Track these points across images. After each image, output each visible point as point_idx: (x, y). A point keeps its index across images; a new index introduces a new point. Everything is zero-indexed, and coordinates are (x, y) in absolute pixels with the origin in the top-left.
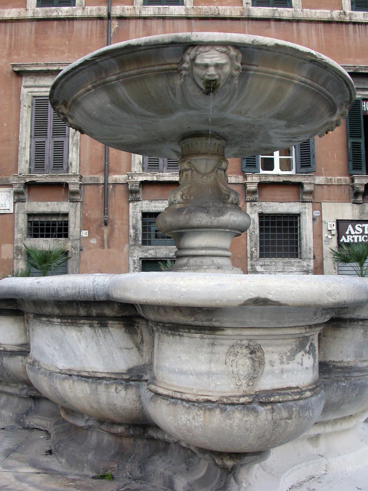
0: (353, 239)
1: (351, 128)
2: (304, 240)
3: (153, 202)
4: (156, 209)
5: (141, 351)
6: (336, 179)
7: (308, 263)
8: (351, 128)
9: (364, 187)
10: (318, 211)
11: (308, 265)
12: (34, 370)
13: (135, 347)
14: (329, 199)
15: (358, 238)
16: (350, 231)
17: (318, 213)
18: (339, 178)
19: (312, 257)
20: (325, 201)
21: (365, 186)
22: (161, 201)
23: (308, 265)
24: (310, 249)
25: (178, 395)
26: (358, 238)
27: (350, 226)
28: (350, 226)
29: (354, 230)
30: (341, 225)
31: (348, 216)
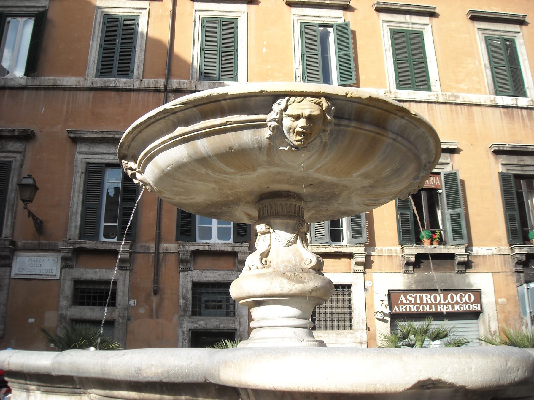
0: (406, 309)
3: (205, 271)
4: (207, 279)
9: (414, 257)
10: (370, 282)
15: (410, 308)
16: (402, 301)
17: (370, 284)
18: (389, 248)
22: (212, 271)
26: (410, 308)
27: (402, 296)
28: (402, 296)
29: (406, 299)
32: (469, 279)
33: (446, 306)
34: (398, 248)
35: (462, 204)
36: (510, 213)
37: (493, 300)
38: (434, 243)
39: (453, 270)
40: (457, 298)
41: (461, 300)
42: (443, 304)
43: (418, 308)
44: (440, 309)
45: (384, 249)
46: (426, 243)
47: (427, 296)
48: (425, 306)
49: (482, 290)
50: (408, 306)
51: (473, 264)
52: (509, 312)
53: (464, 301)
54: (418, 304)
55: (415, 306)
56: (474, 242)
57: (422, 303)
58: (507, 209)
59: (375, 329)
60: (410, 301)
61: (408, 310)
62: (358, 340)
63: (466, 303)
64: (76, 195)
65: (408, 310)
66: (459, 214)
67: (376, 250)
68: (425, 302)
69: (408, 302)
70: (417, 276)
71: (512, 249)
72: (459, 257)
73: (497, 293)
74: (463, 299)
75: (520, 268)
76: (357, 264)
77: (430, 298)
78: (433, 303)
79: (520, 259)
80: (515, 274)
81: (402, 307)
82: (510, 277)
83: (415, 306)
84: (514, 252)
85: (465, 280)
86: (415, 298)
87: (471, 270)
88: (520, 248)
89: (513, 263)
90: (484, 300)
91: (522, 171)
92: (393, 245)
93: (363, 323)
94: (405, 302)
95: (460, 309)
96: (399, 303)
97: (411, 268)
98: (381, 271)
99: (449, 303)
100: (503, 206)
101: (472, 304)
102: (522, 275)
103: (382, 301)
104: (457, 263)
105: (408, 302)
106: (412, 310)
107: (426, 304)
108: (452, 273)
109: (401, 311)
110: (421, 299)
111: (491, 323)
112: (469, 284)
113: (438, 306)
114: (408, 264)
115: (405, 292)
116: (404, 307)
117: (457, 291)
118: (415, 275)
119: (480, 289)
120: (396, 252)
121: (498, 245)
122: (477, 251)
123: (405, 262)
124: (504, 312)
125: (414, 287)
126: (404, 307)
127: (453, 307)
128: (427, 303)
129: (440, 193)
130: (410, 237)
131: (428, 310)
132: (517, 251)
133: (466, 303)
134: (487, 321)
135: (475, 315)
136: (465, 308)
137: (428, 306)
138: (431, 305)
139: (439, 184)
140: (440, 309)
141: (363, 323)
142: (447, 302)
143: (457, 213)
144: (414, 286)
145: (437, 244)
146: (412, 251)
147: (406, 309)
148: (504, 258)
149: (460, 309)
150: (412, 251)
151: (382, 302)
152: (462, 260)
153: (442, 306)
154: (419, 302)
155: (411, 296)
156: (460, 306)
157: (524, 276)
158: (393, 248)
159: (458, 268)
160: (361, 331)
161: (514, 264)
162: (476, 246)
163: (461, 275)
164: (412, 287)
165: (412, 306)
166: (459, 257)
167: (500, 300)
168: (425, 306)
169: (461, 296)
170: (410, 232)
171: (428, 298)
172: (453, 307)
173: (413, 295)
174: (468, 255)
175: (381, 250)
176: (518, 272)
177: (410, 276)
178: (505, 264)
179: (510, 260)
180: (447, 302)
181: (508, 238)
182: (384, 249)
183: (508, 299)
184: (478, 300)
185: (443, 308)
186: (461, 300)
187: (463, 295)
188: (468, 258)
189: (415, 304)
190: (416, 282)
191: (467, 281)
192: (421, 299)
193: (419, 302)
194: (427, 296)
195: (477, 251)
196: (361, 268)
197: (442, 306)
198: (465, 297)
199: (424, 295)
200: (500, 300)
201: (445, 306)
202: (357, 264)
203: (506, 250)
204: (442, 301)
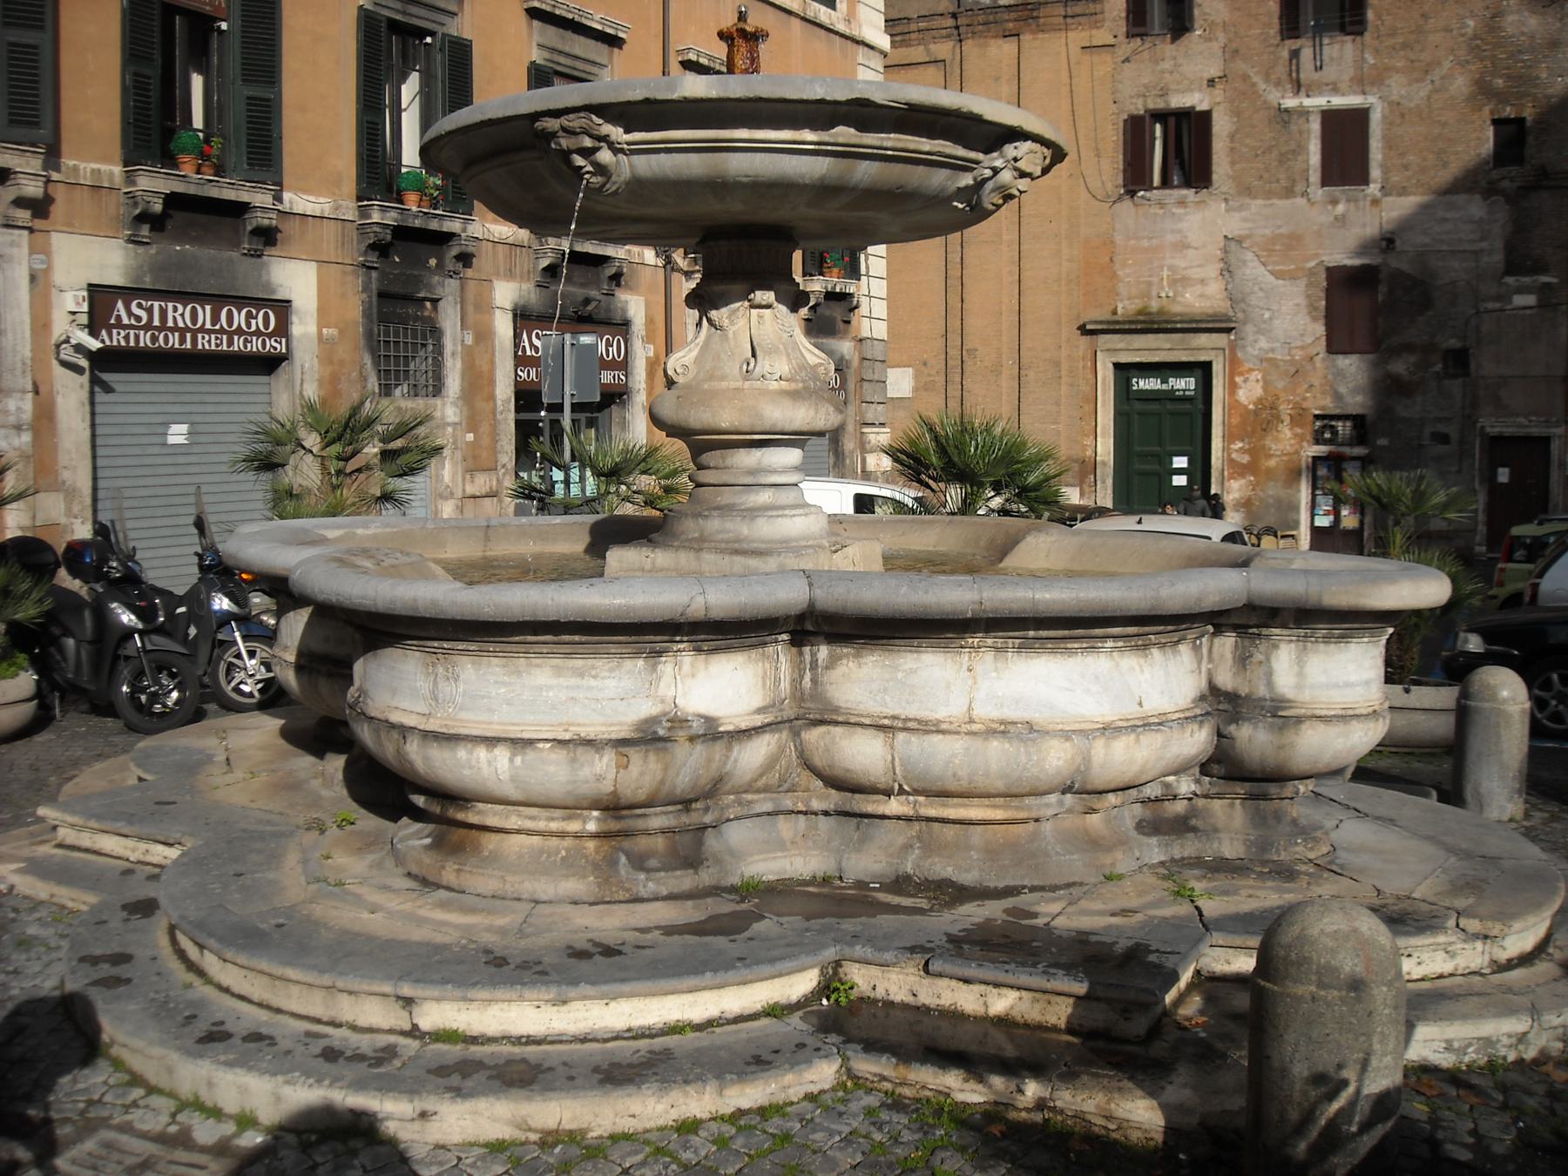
0: (127, 338)
1: (33, 109)
2: (10, 335)
5: (562, 94)
6: (88, 170)
7: (21, 404)
8: (33, 109)
9: (161, 201)
10: (42, 257)
11: (19, 409)
12: (279, 443)
13: (872, 996)
14: (70, 225)
15: (137, 337)
16: (119, 318)
17: (42, 262)
18: (95, 166)
19: (29, 387)
20: (60, 228)
21: (164, 199)
23: (19, 409)
24: (24, 364)
25: (1351, 712)
26: (137, 337)
27: (120, 305)
28: (120, 305)
29: (130, 314)
30: (101, 298)
31: (115, 278)
32: (269, 273)
33: (217, 338)
34: (117, 170)
35: (49, 24)
36: (369, 118)
37: (312, 328)
38: (204, 169)
39: (236, 245)
40: (240, 318)
41: (249, 325)
42: (209, 332)
43: (154, 339)
44: (118, 341)
45: (82, 166)
46: (188, 169)
47: (175, 309)
48: (170, 335)
49: (295, 304)
50: (132, 332)
51: (279, 236)
52: (341, 363)
53: (254, 328)
54: (156, 328)
55: (149, 334)
56: (65, 148)
57: (163, 327)
58: (131, 55)
59: (52, 391)
60: (138, 319)
61: (132, 344)
62: (12, 419)
63: (258, 333)
64: (739, 165)
65: (132, 344)
66: (35, 47)
67: (63, 169)
68: (170, 323)
69: (133, 322)
70: (157, 253)
71: (364, 212)
72: (259, 214)
73: (324, 314)
74: (253, 322)
75: (373, 258)
76: (20, 202)
77: (182, 315)
78: (187, 329)
79: (381, 236)
80: (361, 271)
81: (119, 334)
82: (350, 278)
83: (149, 334)
84: (369, 217)
85: (260, 276)
86: (150, 311)
87: (273, 251)
88: (384, 209)
89: (359, 243)
90: (297, 329)
91: (404, 13)
92: (106, 159)
93: (24, 372)
94: (125, 321)
95: (246, 347)
96: (112, 321)
97: (145, 230)
98: (71, 228)
99: (222, 331)
100: (358, 98)
101: (270, 336)
102: (374, 274)
103: (74, 313)
104: (249, 228)
105: (133, 322)
106: (142, 344)
107: (173, 330)
108: (234, 254)
109: (115, 343)
110: (163, 313)
111: (305, 386)
112: (268, 286)
113: (200, 336)
114: (143, 218)
115: (128, 293)
116: (123, 333)
117: (241, 301)
118: (153, 250)
119: (289, 301)
120: (111, 179)
121: (334, 194)
122: (291, 203)
123: (137, 212)
124: (331, 362)
125: (147, 282)
126: (123, 333)
127: (230, 343)
128: (175, 329)
129: (221, 32)
130: (149, 141)
131: (177, 346)
132: (376, 217)
133: (258, 333)
134: (298, 382)
135: (269, 364)
136: (256, 345)
137: (177, 334)
138: (182, 332)
139: (223, 5)
140: (118, 341)
141: (24, 372)
142: (217, 327)
143: (31, 41)
144: (147, 279)
145: (212, 171)
146: (154, 184)
147: (127, 338)
148: (343, 228)
149: (246, 347)
150: (154, 184)
151: (72, 317)
152: (266, 222)
153: (207, 337)
154: (156, 323)
155: (140, 306)
156: (246, 341)
157: (380, 280)
158: (103, 167)
159: (250, 244)
160: (19, 395)
161: (363, 247)
162: (289, 190)
163: (254, 259)
164: (144, 282)
165: (142, 332)
166: (259, 214)
167: (325, 331)
168: (170, 335)
169: (249, 316)
170: (149, 129)
171: (179, 314)
172: (230, 343)
173: (144, 303)
174: (48, 181)
175: (75, 168)
176: (369, 268)
177: (141, 250)
178: (343, 244)
179: (355, 233)
180: (217, 327)
181: (359, 182)
182: (82, 166)
183: (341, 332)
184: (283, 330)
185: (209, 341)
186: (249, 325)
187: (254, 312)
188: (46, 188)
189: (148, 326)
190: (158, 269)
191: (265, 278)
192: (163, 313)
193: (156, 323)
194: (175, 309)
195: (291, 203)
196: (23, 215)
197: (207, 337)
198: (256, 318)
199: (170, 305)
200: (325, 331)
201: (213, 336)
202: (20, 202)
203: (349, 210)
204: (208, 326)
